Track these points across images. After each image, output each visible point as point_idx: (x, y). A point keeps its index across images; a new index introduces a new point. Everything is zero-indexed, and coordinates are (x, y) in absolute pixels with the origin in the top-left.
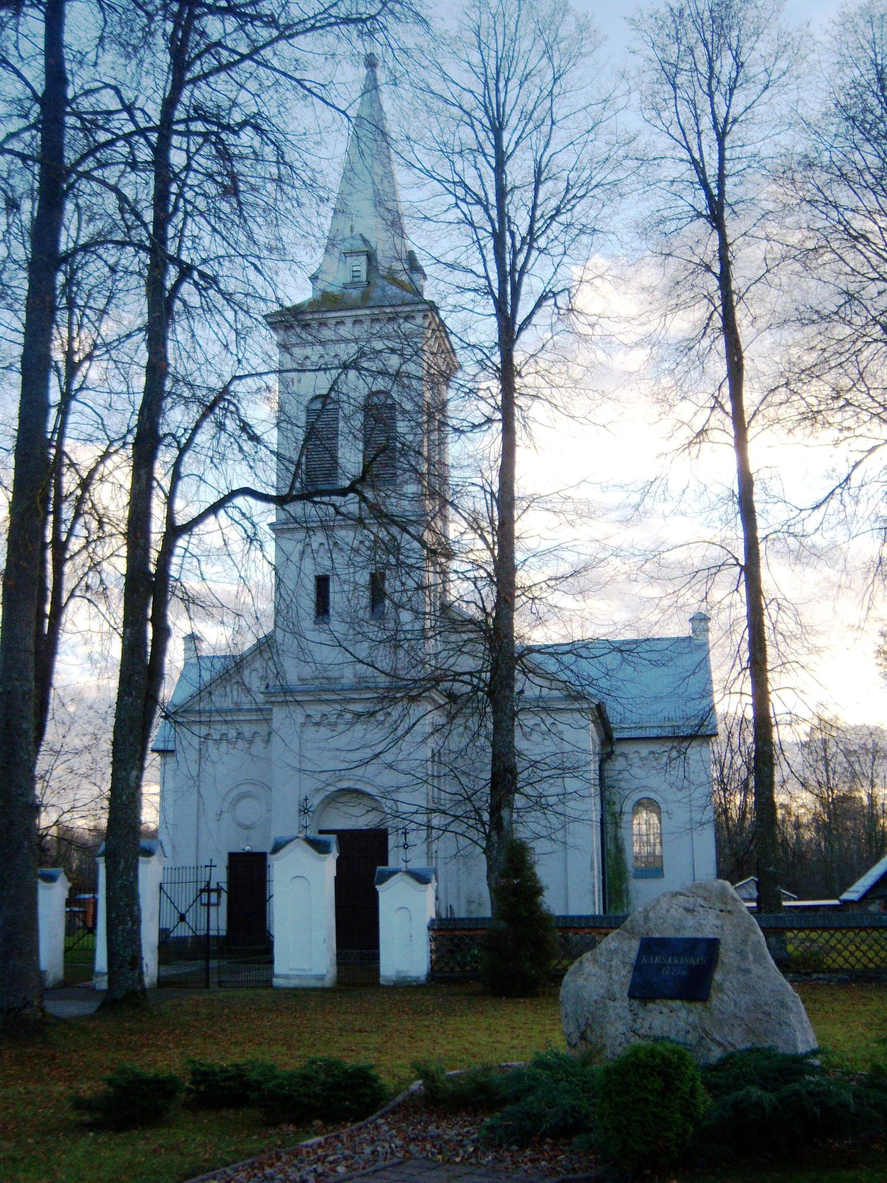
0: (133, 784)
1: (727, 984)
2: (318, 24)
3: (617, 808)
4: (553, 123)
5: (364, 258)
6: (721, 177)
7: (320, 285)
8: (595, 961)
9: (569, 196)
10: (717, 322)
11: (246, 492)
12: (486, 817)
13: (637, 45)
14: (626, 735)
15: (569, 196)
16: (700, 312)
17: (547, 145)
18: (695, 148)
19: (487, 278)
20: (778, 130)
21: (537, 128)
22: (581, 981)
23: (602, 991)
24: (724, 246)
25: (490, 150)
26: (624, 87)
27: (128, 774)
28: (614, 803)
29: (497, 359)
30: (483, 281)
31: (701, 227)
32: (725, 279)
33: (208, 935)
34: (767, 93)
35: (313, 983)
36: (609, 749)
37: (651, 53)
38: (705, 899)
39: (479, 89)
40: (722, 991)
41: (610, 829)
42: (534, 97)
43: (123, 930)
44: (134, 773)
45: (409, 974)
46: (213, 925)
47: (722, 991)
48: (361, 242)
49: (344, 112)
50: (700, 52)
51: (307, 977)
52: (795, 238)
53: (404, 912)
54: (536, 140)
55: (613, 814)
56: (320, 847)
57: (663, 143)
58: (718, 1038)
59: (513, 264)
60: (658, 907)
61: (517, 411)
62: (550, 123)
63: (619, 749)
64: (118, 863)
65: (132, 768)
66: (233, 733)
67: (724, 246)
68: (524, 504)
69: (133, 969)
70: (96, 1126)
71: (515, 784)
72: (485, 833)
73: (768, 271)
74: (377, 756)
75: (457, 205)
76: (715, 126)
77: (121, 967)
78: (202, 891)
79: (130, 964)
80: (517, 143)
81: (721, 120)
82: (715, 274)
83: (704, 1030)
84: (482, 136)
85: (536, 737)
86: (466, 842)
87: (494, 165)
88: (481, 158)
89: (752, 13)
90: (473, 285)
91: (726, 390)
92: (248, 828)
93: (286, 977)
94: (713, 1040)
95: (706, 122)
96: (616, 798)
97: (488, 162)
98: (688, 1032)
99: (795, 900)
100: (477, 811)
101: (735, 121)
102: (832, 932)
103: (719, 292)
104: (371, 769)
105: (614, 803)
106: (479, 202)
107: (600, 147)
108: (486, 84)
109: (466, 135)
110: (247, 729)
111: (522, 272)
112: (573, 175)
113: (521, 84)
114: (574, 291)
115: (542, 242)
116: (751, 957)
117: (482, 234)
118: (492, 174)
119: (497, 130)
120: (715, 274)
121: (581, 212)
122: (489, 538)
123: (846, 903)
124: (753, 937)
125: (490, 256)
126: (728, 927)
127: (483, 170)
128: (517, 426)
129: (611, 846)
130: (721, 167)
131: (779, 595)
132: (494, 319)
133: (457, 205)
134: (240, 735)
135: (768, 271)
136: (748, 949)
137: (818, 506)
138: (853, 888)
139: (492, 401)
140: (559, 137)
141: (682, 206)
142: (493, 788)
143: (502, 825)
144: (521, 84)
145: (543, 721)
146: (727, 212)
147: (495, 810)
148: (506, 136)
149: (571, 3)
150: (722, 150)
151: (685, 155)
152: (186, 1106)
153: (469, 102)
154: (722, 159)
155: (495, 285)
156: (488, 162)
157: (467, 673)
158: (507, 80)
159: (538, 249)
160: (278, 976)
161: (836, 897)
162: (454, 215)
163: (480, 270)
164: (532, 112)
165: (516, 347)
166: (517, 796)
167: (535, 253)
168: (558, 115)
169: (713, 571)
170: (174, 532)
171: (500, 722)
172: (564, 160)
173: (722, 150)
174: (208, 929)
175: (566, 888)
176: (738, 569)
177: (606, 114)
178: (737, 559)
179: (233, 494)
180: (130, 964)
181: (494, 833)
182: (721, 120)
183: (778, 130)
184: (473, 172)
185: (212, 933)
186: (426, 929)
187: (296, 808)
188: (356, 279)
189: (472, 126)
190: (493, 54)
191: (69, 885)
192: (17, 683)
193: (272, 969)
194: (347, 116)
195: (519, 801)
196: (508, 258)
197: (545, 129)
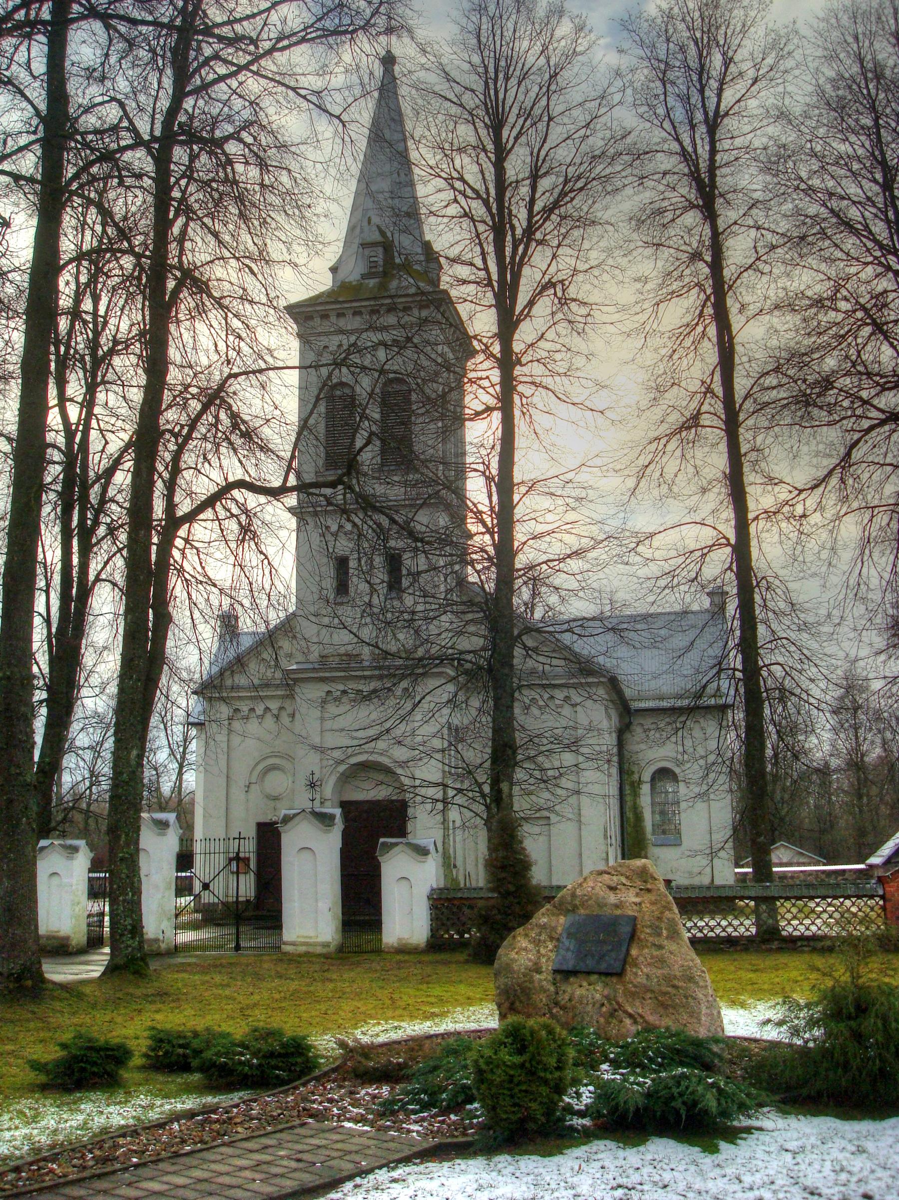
0: (133, 763)
1: (641, 959)
2: (309, 36)
3: (636, 777)
4: (550, 119)
5: (380, 250)
6: (712, 168)
7: (341, 275)
8: (526, 935)
9: (567, 188)
10: (709, 310)
11: (241, 484)
12: (487, 789)
13: (626, 45)
14: (643, 705)
15: (567, 188)
16: (693, 299)
17: (544, 142)
18: (687, 142)
19: (486, 269)
20: (765, 122)
21: (534, 124)
22: (513, 955)
23: (530, 964)
24: (716, 235)
25: (490, 147)
26: (619, 83)
27: (129, 753)
28: (633, 772)
29: (496, 349)
30: (482, 274)
31: (692, 218)
32: (716, 266)
33: (237, 902)
34: (756, 87)
35: (319, 950)
36: (627, 720)
37: (641, 52)
38: (627, 877)
39: (480, 87)
40: (636, 965)
41: (628, 799)
42: (532, 95)
43: (124, 901)
44: (135, 753)
45: (410, 941)
46: (242, 891)
47: (636, 965)
48: (377, 233)
49: (338, 117)
50: (692, 51)
51: (315, 944)
52: (783, 226)
53: (404, 882)
54: (533, 136)
55: (632, 784)
56: (325, 819)
57: (658, 135)
58: (630, 1010)
59: (513, 257)
60: (585, 885)
61: (516, 398)
62: (546, 119)
63: (636, 721)
64: (119, 837)
65: (133, 747)
66: (260, 710)
67: (716, 235)
68: (523, 489)
69: (133, 938)
70: (44, 1088)
71: (515, 758)
72: (486, 806)
73: (758, 259)
74: (388, 731)
75: (456, 201)
76: (706, 120)
77: (122, 935)
78: (231, 860)
79: (131, 932)
80: (516, 139)
81: (711, 114)
82: (706, 262)
83: (618, 1003)
84: (483, 132)
85: (535, 711)
86: (469, 814)
87: (493, 159)
88: (482, 155)
89: (738, 13)
90: (473, 277)
91: (717, 377)
92: (276, 799)
93: (293, 944)
94: (626, 1012)
95: (699, 116)
96: (635, 769)
97: (489, 158)
98: (603, 1005)
99: (824, 865)
100: (480, 785)
101: (727, 114)
102: (854, 900)
103: (711, 282)
104: (381, 745)
105: (633, 772)
106: (479, 197)
107: (597, 142)
108: (486, 83)
109: (465, 133)
110: (274, 705)
111: (521, 264)
112: (571, 170)
113: (519, 84)
114: (567, 283)
115: (538, 236)
116: (665, 933)
117: (481, 228)
118: (492, 170)
119: (497, 126)
120: (706, 262)
121: (578, 204)
122: (488, 520)
123: (871, 866)
124: (667, 914)
125: (490, 249)
126: (646, 907)
127: (484, 166)
128: (517, 413)
129: (630, 815)
130: (712, 160)
131: (770, 573)
132: (494, 310)
133: (456, 201)
134: (267, 709)
135: (758, 259)
136: (663, 925)
137: (816, 486)
138: (879, 852)
139: (491, 390)
140: (557, 133)
141: (675, 198)
142: (493, 763)
143: (501, 798)
144: (519, 84)
145: (541, 697)
146: (719, 201)
147: (495, 782)
148: (505, 133)
149: (566, 5)
150: (713, 143)
151: (675, 147)
152: (142, 1068)
153: (470, 100)
154: (713, 151)
155: (495, 277)
156: (489, 158)
157: (470, 652)
158: (507, 79)
159: (537, 241)
160: (285, 943)
161: (863, 862)
162: (453, 210)
163: (479, 262)
164: (532, 108)
165: (516, 337)
166: (518, 770)
167: (534, 244)
168: (556, 110)
169: (705, 551)
170: (173, 522)
171: (500, 699)
172: (564, 154)
173: (713, 143)
174: (237, 897)
175: (580, 855)
176: (728, 550)
177: (603, 110)
178: (728, 540)
179: (230, 486)
180: (131, 932)
181: (493, 806)
182: (711, 114)
183: (765, 122)
184: (475, 168)
185: (241, 899)
186: (426, 899)
187: (304, 782)
188: (373, 270)
189: (474, 124)
190: (492, 54)
191: (92, 855)
192: (16, 670)
193: (280, 935)
194: (341, 121)
195: (519, 774)
196: (508, 251)
197: (541, 126)
